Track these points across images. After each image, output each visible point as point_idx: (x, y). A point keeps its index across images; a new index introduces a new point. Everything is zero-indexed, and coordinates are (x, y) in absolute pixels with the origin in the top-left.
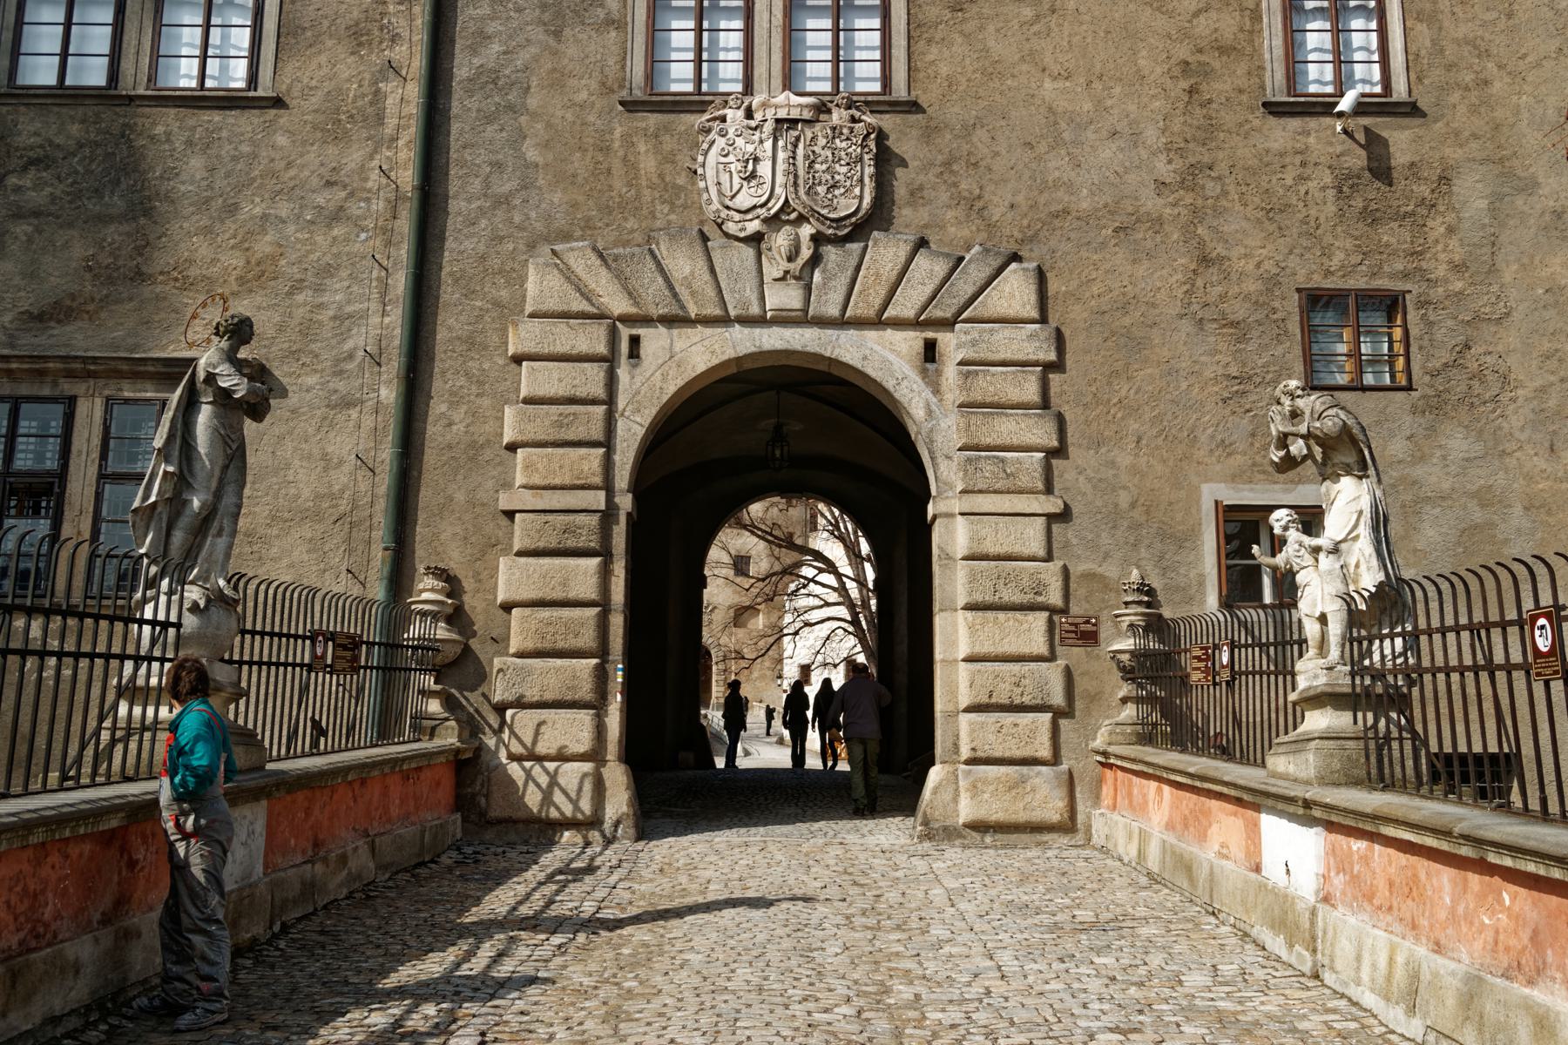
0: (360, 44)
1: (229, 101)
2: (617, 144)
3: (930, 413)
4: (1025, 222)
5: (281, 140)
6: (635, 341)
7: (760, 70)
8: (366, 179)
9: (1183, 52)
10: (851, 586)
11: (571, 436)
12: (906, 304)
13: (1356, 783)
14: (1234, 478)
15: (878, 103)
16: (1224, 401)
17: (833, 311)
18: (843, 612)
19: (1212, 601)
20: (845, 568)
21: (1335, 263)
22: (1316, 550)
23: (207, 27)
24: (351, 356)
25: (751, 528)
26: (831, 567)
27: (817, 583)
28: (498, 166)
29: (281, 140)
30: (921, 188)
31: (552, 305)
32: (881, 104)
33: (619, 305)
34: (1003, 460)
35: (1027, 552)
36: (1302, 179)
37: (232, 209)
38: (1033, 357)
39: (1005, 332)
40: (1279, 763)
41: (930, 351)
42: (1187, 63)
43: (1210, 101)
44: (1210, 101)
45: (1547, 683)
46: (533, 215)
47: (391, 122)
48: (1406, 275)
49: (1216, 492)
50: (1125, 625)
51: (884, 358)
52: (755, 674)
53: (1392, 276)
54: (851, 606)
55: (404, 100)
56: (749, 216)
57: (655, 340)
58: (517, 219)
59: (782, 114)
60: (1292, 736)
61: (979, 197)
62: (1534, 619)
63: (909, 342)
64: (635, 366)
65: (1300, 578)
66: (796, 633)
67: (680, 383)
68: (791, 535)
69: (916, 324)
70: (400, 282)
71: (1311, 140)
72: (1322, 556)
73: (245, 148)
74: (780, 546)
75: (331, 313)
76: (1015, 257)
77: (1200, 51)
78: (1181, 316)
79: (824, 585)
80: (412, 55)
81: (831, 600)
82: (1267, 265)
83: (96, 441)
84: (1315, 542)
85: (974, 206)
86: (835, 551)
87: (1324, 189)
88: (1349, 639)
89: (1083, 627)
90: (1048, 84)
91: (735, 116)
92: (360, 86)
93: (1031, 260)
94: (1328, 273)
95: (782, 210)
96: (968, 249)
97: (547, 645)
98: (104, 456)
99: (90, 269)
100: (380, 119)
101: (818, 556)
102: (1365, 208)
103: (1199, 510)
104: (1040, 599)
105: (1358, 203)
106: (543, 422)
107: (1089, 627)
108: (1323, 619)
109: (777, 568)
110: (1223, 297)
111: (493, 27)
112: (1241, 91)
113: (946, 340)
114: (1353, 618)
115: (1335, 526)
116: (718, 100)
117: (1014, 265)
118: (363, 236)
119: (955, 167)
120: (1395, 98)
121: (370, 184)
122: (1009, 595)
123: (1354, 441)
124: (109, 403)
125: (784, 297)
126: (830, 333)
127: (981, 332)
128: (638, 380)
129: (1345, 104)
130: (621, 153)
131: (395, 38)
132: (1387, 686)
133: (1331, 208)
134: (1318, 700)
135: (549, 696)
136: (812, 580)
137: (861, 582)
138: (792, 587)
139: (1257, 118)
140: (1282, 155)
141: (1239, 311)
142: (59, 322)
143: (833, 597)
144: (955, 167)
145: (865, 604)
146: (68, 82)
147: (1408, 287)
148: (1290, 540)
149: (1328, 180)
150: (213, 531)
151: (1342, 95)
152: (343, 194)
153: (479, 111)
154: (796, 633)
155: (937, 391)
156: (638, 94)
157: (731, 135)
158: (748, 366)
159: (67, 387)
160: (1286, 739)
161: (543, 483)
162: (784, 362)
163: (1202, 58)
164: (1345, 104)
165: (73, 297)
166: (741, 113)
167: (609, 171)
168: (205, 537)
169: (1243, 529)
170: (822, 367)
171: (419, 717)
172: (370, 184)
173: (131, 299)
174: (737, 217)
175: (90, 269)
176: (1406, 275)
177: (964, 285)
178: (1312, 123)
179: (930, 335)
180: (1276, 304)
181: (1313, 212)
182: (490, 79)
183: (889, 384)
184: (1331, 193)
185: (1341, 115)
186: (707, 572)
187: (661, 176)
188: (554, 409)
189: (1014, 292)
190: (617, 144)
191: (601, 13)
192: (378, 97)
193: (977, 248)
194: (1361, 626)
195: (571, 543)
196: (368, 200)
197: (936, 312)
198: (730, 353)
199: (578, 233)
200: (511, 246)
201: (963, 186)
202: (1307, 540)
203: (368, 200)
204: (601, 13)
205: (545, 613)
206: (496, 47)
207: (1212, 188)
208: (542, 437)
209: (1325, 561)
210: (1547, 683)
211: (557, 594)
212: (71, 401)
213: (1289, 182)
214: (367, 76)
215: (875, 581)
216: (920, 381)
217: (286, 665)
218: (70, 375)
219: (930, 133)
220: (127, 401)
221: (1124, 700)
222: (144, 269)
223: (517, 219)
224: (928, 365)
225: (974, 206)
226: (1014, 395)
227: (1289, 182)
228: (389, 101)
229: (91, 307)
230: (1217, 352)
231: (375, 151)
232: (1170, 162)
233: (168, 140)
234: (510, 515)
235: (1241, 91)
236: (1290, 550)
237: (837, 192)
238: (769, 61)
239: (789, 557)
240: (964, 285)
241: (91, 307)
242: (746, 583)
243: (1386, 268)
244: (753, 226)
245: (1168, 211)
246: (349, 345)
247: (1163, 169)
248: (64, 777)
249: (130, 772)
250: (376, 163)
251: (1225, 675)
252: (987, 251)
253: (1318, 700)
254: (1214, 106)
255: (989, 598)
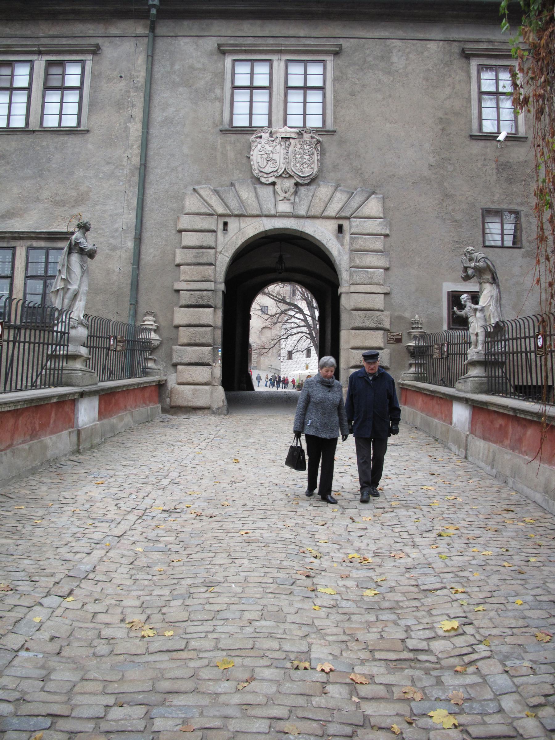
0: (120, 108)
1: (70, 131)
2: (219, 147)
3: (339, 253)
4: (378, 179)
5: (90, 146)
6: (225, 224)
7: (274, 118)
8: (122, 161)
9: (440, 114)
10: (309, 319)
11: (201, 261)
12: (332, 211)
13: (481, 392)
14: (454, 281)
15: (321, 131)
16: (453, 250)
17: (303, 213)
18: (305, 329)
19: (445, 327)
20: (307, 311)
21: (496, 198)
22: (476, 310)
23: (62, 103)
24: (117, 230)
25: (269, 295)
26: (301, 311)
27: (295, 317)
28: (173, 155)
29: (90, 146)
30: (337, 165)
31: (194, 210)
32: (322, 131)
33: (221, 210)
34: (367, 272)
35: (376, 307)
36: (484, 165)
37: (72, 173)
38: (380, 232)
39: (370, 222)
40: (459, 385)
41: (340, 229)
42: (441, 119)
43: (450, 134)
44: (450, 134)
45: (541, 357)
46: (186, 174)
47: (132, 138)
48: (521, 204)
49: (450, 286)
50: (412, 336)
51: (322, 232)
52: (270, 354)
53: (517, 204)
54: (308, 325)
55: (136, 128)
56: (270, 175)
57: (233, 224)
58: (180, 176)
59: (283, 136)
60: (463, 377)
61: (360, 169)
62: (538, 335)
63: (332, 225)
64: (225, 234)
65: (470, 320)
66: (286, 338)
67: (243, 240)
68: (285, 297)
69: (336, 218)
70: (134, 201)
71: (488, 150)
72: (478, 313)
73: (77, 150)
74: (280, 302)
75: (109, 213)
76: (373, 193)
77: (447, 114)
78: (437, 217)
79: (298, 319)
80: (138, 112)
81: (301, 325)
82: (470, 198)
83: (24, 264)
84: (477, 306)
85: (358, 172)
86: (303, 305)
87: (492, 169)
88: (486, 342)
89: (397, 337)
90: (388, 125)
91: (265, 136)
92: (120, 125)
93: (380, 194)
94: (493, 202)
95: (283, 173)
96: (356, 189)
97: (192, 341)
98: (27, 269)
99: (20, 198)
100: (127, 137)
101: (296, 307)
102: (508, 177)
103: (442, 293)
104: (380, 326)
105: (505, 175)
106: (189, 257)
107: (398, 337)
108: (477, 335)
109: (279, 311)
110: (453, 210)
111: (170, 101)
112: (462, 130)
113: (345, 223)
114: (488, 335)
115: (483, 302)
116: (259, 129)
117: (373, 196)
118: (121, 183)
119: (351, 157)
120: (520, 135)
121: (124, 163)
122: (369, 324)
123: (490, 270)
124: (29, 249)
125: (284, 207)
126: (302, 221)
127: (360, 222)
128: (227, 239)
129: (501, 137)
130: (221, 150)
131: (133, 106)
132: (495, 359)
133: (495, 177)
134: (474, 364)
135: (193, 361)
136: (293, 316)
137: (313, 318)
138: (285, 319)
139: (468, 142)
140: (477, 156)
141: (458, 217)
142: (9, 218)
143: (302, 323)
144: (351, 157)
145: (315, 328)
146: (11, 126)
147: (522, 208)
148: (467, 306)
149: (494, 166)
150: (78, 299)
151: (500, 133)
152: (113, 167)
153: (165, 134)
154: (286, 338)
155: (342, 245)
156: (227, 127)
157: (263, 143)
158: (269, 234)
159: (13, 243)
160: (463, 377)
161: (191, 279)
162: (284, 232)
163: (447, 117)
164: (501, 137)
165: (14, 209)
166: (268, 135)
167: (216, 157)
168: (75, 302)
169: (455, 299)
170: (298, 234)
171: (145, 368)
172: (124, 163)
173: (35, 209)
174: (266, 176)
175: (20, 198)
176: (521, 204)
177: (354, 204)
178: (489, 143)
179: (341, 222)
180: (473, 214)
181: (488, 178)
182: (169, 121)
183: (324, 242)
184: (495, 171)
185: (499, 141)
186: (251, 313)
187: (236, 159)
188: (194, 250)
189: (373, 206)
190: (219, 147)
191: (213, 95)
192: (126, 129)
193: (359, 189)
194: (489, 337)
195: (201, 302)
196: (123, 169)
197: (343, 214)
198: (262, 229)
199: (204, 182)
200: (177, 187)
201: (354, 164)
202: (474, 306)
203: (123, 169)
204: (213, 95)
205: (192, 329)
206: (172, 109)
207: (450, 168)
208: (190, 261)
209: (478, 314)
210: (541, 357)
211: (196, 322)
212: (14, 248)
213: (479, 166)
214: (122, 121)
215: (319, 317)
216: (335, 240)
217: (525, 338)
218: (14, 238)
219: (342, 142)
220: (35, 248)
221: (411, 365)
222: (40, 198)
223: (180, 176)
224: (340, 235)
225: (358, 172)
226: (373, 247)
227: (479, 166)
228: (131, 131)
229: (20, 212)
230: (450, 231)
231: (125, 150)
232: (434, 157)
233: (48, 148)
234: (178, 291)
235: (462, 130)
236: (467, 309)
237: (305, 166)
238: (278, 115)
239: (284, 307)
240: (354, 204)
241: (20, 212)
242: (266, 317)
243: (515, 201)
244: (271, 180)
245: (433, 176)
246: (116, 226)
247: (431, 160)
248: (32, 386)
249: (55, 383)
250: (126, 155)
251: (445, 355)
252: (363, 190)
253: (474, 364)
254: (451, 136)
255: (361, 325)
